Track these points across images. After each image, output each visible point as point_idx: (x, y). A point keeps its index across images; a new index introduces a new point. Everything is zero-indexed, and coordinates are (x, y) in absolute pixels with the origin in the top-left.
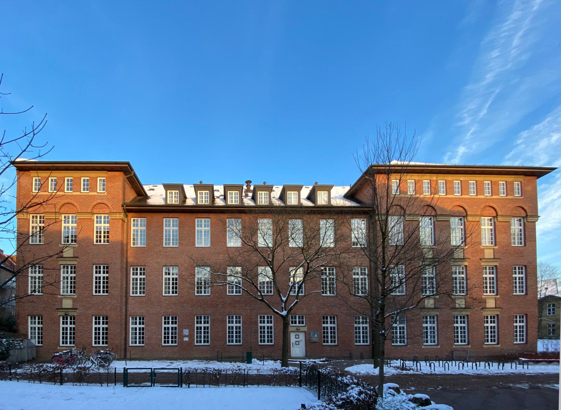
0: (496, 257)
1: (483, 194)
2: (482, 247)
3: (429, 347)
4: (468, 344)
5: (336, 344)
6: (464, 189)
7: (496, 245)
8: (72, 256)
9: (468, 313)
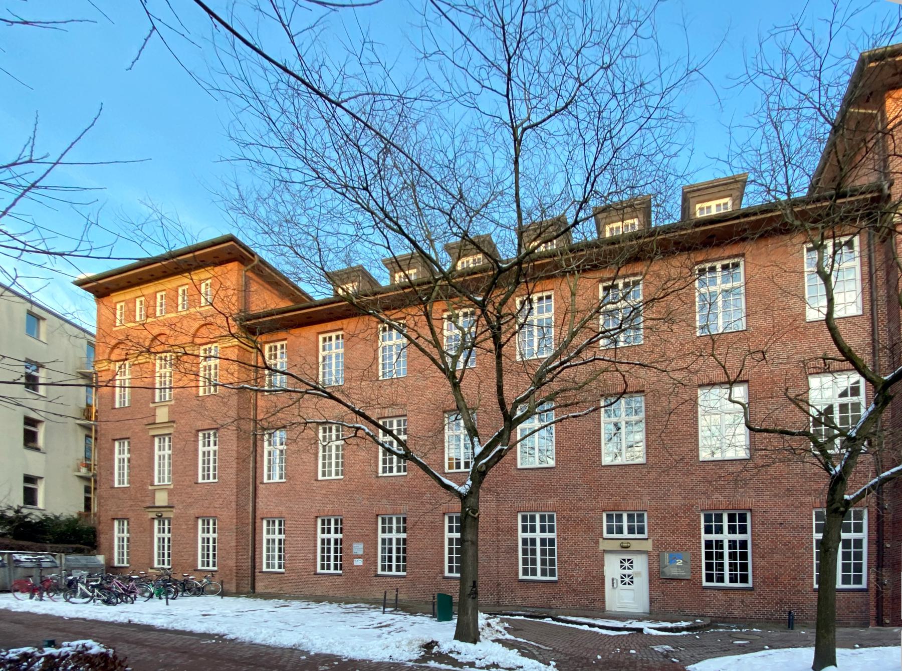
5: (750, 584)
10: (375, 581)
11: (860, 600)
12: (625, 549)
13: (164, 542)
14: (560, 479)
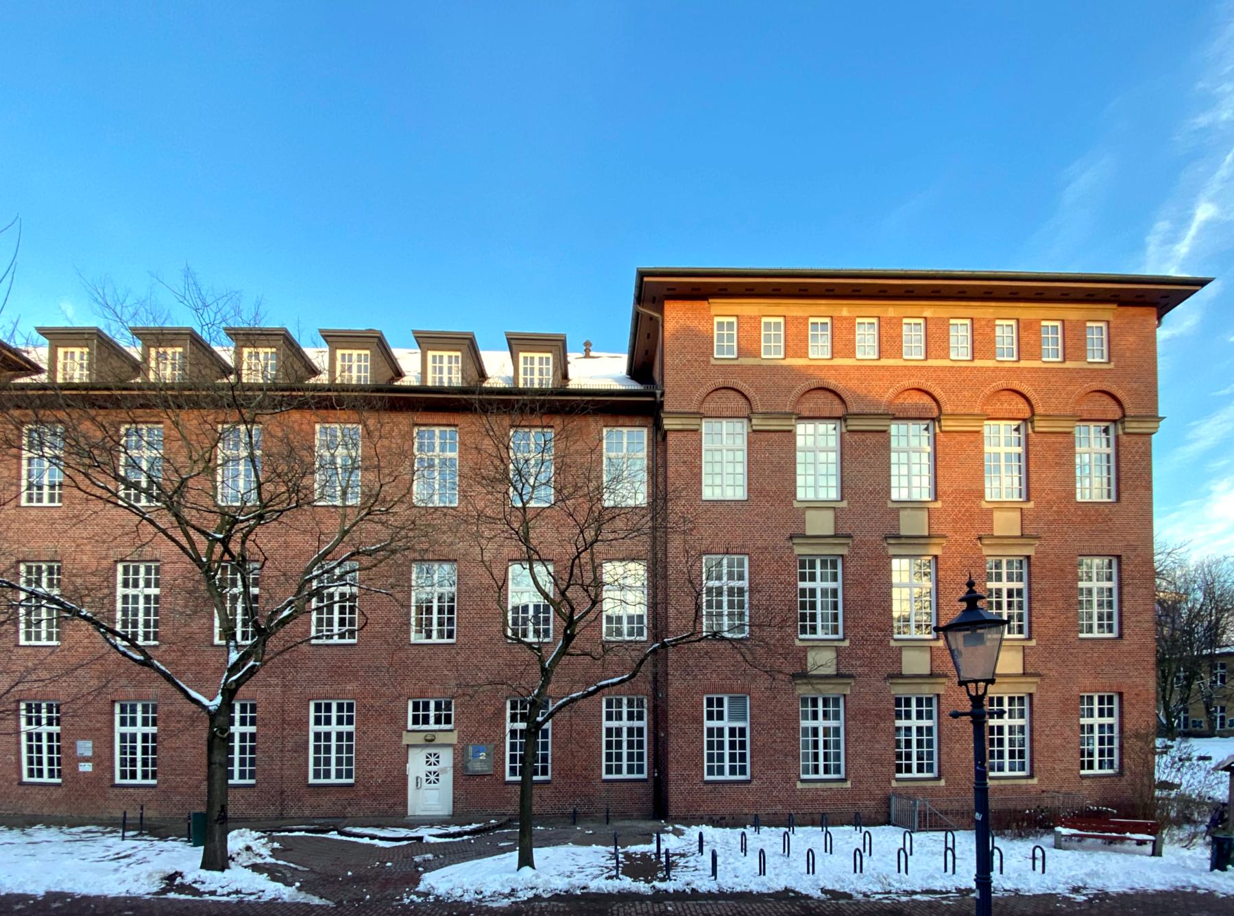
0: (1027, 532)
1: (993, 356)
2: (984, 505)
3: (819, 785)
4: (1031, 776)
6: (936, 341)
7: (1028, 500)
8: (832, 533)
9: (941, 690)
10: (112, 793)
11: (642, 791)
12: (429, 742)
14: (362, 659)
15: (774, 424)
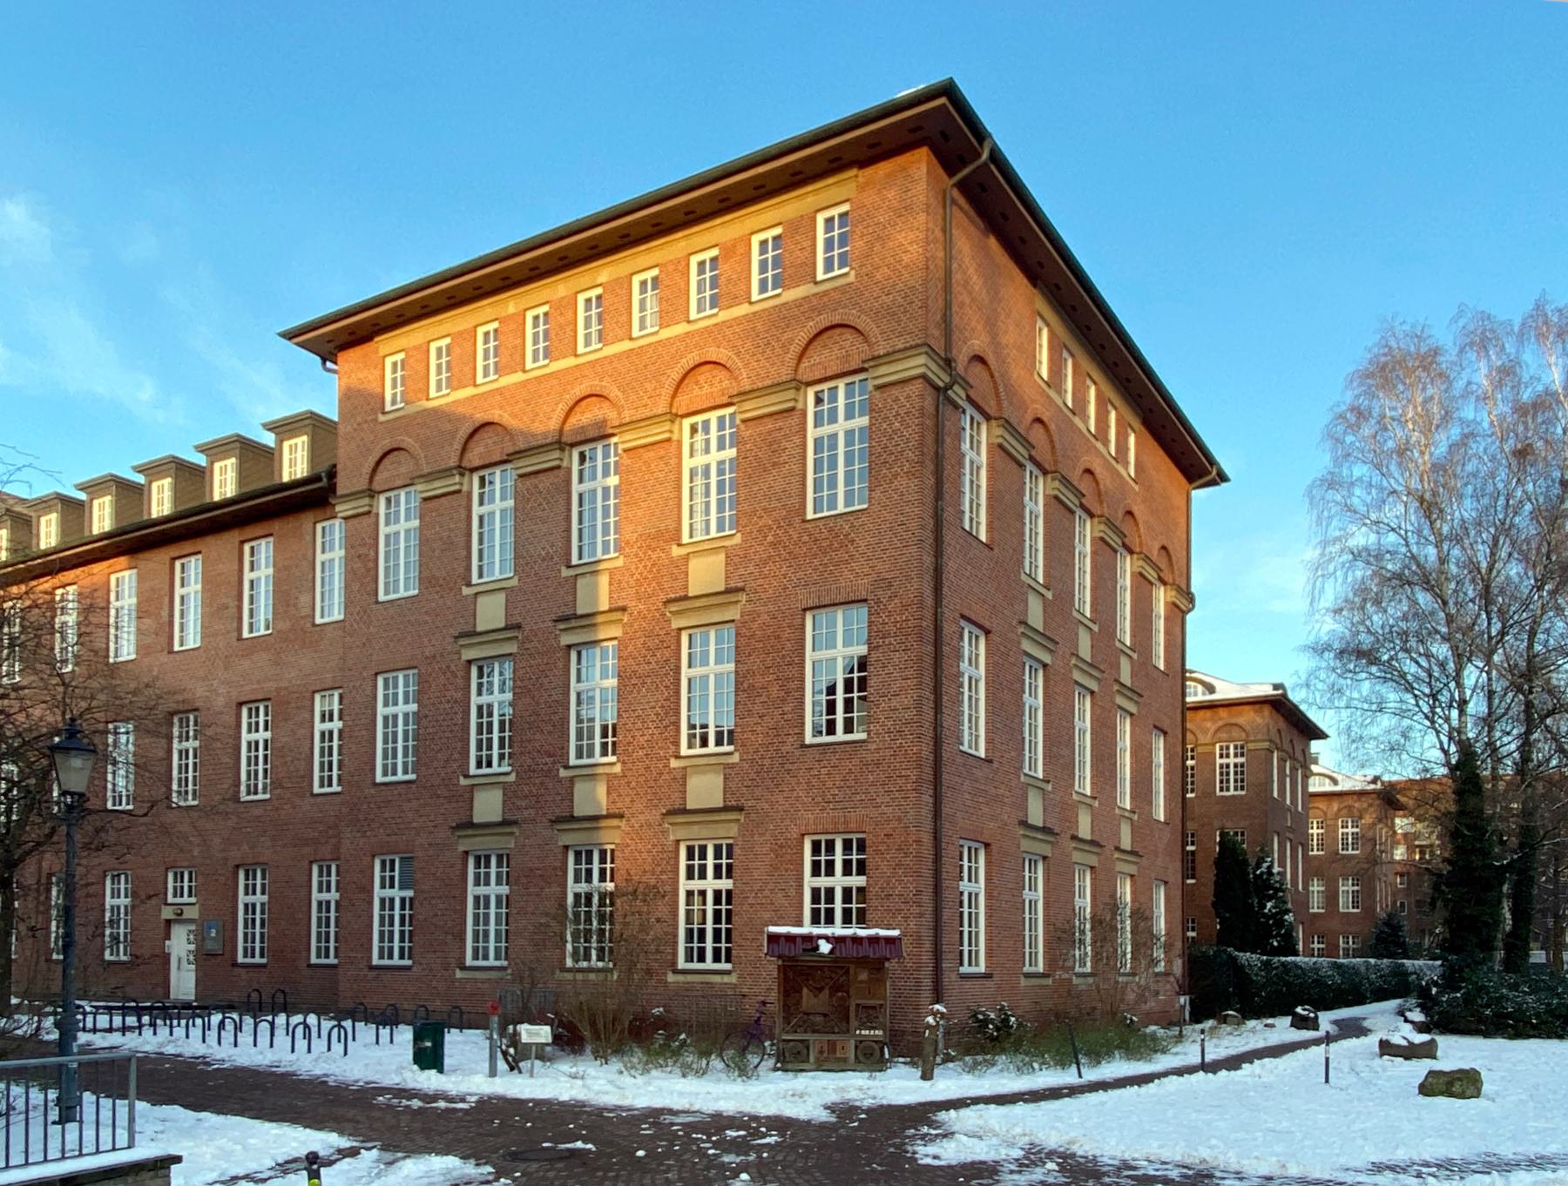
13: (487, 906)
15: (439, 487)
